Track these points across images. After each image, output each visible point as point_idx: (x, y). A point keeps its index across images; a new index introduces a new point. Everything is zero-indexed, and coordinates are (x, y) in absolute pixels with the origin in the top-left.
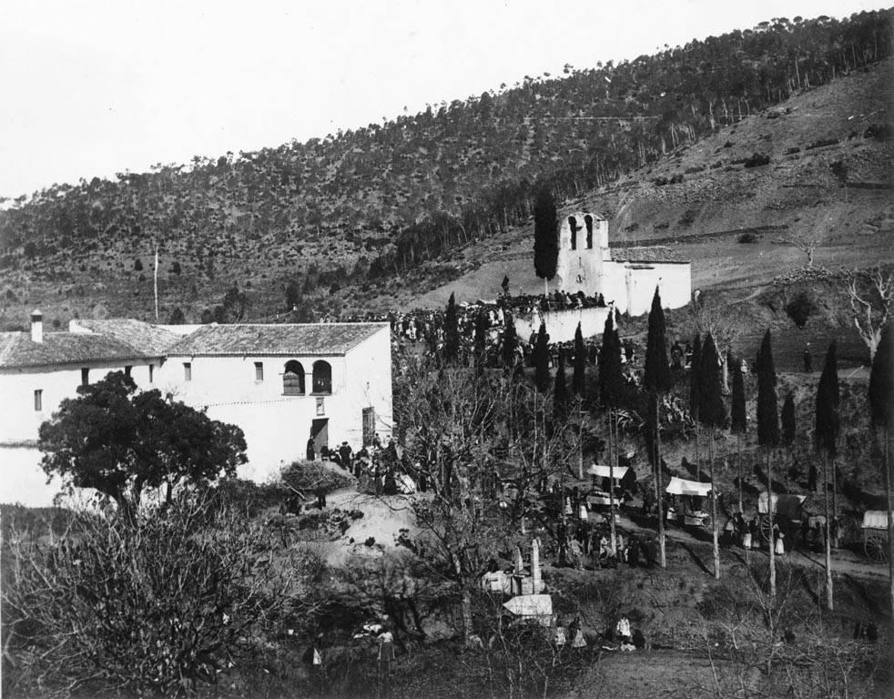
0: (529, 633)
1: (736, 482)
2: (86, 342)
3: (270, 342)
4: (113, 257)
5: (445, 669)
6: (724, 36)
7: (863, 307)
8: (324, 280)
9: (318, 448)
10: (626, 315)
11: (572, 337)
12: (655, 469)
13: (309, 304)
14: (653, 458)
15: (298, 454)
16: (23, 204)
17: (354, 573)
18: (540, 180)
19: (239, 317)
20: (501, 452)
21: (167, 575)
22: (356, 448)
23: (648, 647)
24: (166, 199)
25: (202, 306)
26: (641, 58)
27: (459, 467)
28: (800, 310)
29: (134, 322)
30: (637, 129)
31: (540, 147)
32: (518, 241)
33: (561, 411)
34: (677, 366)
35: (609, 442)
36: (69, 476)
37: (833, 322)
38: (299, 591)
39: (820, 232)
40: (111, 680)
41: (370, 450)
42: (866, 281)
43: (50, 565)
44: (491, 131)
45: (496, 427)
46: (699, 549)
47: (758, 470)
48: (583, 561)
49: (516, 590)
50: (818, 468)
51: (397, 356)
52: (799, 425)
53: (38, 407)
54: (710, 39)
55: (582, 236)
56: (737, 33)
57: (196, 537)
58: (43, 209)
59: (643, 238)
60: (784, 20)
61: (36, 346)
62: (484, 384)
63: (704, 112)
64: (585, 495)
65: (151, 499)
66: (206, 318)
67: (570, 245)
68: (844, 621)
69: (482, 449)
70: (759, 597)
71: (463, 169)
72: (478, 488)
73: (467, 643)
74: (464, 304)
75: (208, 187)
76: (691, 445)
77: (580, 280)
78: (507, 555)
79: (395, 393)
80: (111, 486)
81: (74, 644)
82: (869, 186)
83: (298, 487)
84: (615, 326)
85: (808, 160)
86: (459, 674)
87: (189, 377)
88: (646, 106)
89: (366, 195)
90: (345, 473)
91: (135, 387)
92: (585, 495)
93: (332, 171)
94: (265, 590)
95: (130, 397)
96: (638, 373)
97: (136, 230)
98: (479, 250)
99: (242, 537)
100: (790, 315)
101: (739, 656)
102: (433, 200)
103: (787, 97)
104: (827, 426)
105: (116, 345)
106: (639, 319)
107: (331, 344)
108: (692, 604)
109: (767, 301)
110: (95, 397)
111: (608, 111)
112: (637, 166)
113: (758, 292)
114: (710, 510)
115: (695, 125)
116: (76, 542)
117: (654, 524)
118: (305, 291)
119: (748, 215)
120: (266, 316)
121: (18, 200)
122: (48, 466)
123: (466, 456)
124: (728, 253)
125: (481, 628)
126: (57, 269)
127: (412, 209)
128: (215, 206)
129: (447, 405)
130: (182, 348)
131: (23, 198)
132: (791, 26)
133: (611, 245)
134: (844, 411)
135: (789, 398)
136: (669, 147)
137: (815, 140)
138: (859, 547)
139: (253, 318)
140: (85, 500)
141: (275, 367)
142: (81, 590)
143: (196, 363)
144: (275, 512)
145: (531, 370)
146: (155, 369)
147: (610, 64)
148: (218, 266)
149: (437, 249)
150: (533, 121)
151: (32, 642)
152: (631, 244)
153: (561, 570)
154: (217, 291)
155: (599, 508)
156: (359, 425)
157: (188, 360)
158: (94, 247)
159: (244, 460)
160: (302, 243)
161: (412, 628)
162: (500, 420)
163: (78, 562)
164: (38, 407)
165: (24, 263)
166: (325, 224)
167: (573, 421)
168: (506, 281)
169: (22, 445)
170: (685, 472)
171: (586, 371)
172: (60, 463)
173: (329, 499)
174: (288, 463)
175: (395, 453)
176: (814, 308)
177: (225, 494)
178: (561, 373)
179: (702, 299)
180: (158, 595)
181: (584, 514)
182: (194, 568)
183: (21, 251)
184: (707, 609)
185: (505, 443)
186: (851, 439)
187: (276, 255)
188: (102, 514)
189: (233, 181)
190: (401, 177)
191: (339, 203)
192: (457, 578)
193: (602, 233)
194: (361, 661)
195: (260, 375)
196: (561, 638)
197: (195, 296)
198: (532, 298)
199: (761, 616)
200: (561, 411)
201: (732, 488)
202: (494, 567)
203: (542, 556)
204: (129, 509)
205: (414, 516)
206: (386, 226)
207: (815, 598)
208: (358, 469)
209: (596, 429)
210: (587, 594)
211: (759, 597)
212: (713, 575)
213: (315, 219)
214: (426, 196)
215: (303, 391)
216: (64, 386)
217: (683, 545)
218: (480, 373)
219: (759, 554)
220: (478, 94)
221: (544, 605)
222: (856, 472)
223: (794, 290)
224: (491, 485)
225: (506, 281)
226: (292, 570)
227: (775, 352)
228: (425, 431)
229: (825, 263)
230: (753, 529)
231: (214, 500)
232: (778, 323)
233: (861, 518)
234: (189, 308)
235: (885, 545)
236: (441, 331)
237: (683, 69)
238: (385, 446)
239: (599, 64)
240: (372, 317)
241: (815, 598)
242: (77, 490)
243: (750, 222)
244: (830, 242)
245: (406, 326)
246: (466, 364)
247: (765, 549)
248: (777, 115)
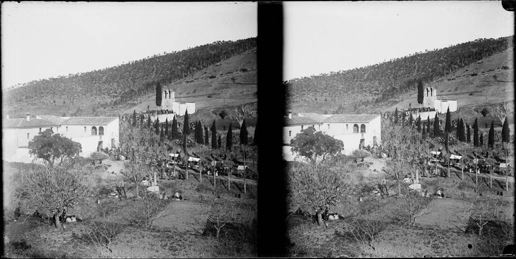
0: (153, 196)
1: (206, 158)
2: (41, 121)
4: (48, 99)
5: (394, 203)
6: (205, 45)
7: (239, 114)
8: (102, 106)
9: (100, 149)
11: (427, 119)
12: (186, 155)
13: (98, 112)
14: (447, 149)
15: (95, 150)
16: (25, 85)
17: (109, 181)
18: (419, 79)
19: (80, 115)
20: (147, 150)
21: (61, 181)
22: (372, 147)
23: (445, 197)
24: (62, 84)
25: (332, 110)
27: (398, 151)
28: (222, 115)
30: (182, 68)
31: (419, 70)
32: (151, 96)
33: (424, 138)
34: (191, 128)
35: (174, 147)
36: (36, 155)
37: (231, 118)
38: (95, 185)
39: (228, 95)
40: (309, 205)
41: (375, 147)
42: (239, 107)
43: (31, 178)
44: (145, 69)
45: (146, 144)
46: (459, 173)
47: (473, 153)
48: (429, 175)
49: (150, 185)
50: (489, 152)
51: (120, 125)
52: (222, 144)
53: (28, 137)
54: (463, 44)
56: (208, 44)
57: (68, 171)
58: (30, 87)
59: (183, 96)
60: (481, 39)
61: (28, 122)
62: (405, 130)
63: (461, 62)
64: (168, 161)
65: (57, 161)
66: (72, 115)
67: (430, 95)
68: (233, 193)
69: (142, 149)
70: (211, 187)
71: (138, 78)
72: (141, 159)
73: (400, 196)
74: (400, 110)
75: (334, 79)
76: (195, 149)
77: (429, 104)
78: (410, 174)
79: (382, 132)
80: (47, 158)
81: (37, 198)
82: (241, 84)
83: (95, 160)
84: (176, 118)
85: (487, 75)
86: (398, 204)
87: (329, 128)
88: (446, 60)
89: (113, 84)
90: (107, 155)
91: (53, 133)
92: (168, 161)
93: (104, 79)
94: (86, 184)
95: (314, 133)
96: (443, 128)
97: (316, 90)
98: (142, 99)
99: (343, 169)
100: (220, 116)
101: (206, 202)
102: (130, 86)
103: (482, 58)
104: (491, 142)
105: (309, 119)
106: (444, 114)
107: (366, 120)
108: (194, 189)
109: (214, 113)
110: (43, 135)
111: (175, 63)
112: (182, 78)
113: (212, 110)
114: (199, 165)
115: (459, 65)
116: (38, 172)
117: (447, 166)
118: (359, 107)
119: (472, 88)
120: (87, 115)
121: (24, 84)
122: (31, 153)
123: (138, 151)
124: (205, 100)
125: (403, 192)
126: (34, 102)
127: (386, 86)
128: (74, 87)
129: (133, 138)
131: (25, 84)
132: (483, 41)
133: (175, 98)
134: (496, 138)
135: (220, 137)
136: (190, 73)
137: (227, 72)
138: (236, 175)
139: (84, 115)
140: (40, 161)
141: (89, 128)
142: (38, 184)
143: (69, 127)
144: (89, 165)
145: (417, 127)
146: (59, 128)
148: (336, 99)
149: (131, 98)
150: (418, 64)
151: (26, 198)
152: (180, 97)
153: (423, 178)
154: (75, 108)
155: (171, 164)
156: (110, 143)
157: (67, 126)
158: (43, 96)
159: (81, 151)
160: (97, 96)
161: (385, 192)
162: (147, 142)
163: (38, 177)
164: (28, 137)
165: (25, 100)
166: (364, 89)
167: (165, 142)
168: (148, 107)
169: (24, 147)
170: (193, 155)
171: (430, 127)
172: (34, 152)
173: (364, 159)
174: (93, 152)
175: (119, 150)
176: (226, 114)
177: (76, 160)
178: (162, 130)
179: (198, 112)
180: (59, 186)
181: (167, 166)
182: (68, 179)
183: (24, 97)
184: (460, 188)
185: (148, 148)
186: (235, 147)
187: (90, 99)
188: (307, 163)
189: (341, 78)
190: (122, 80)
191: (368, 84)
192: (135, 182)
193: (435, 92)
194: (110, 203)
195: (347, 128)
196: (161, 197)
197: (69, 109)
198: (417, 109)
199: (474, 190)
200: (424, 138)
201: (467, 157)
202: (144, 179)
203: (157, 176)
204: (51, 164)
205: (124, 166)
206: (118, 92)
207: (225, 187)
208: (372, 152)
209: (171, 145)
210: (169, 186)
211: (211, 187)
212: (462, 179)
213: (100, 90)
214: (390, 82)
215: (358, 132)
216: (35, 132)
217: (454, 172)
218: (142, 130)
219: (212, 176)
220: (142, 59)
221: (419, 186)
222: (236, 156)
223: (222, 110)
224: (144, 158)
225: (148, 107)
226: (93, 180)
227: (216, 125)
228: (127, 144)
229: (229, 103)
230: (472, 167)
231: (336, 159)
232: (217, 118)
233: (237, 167)
234: (68, 113)
235: (243, 174)
236: (132, 119)
237: (456, 51)
238: (379, 146)
240: (114, 115)
241: (488, 185)
242: (38, 159)
243: (210, 92)
244: (231, 97)
245: (123, 118)
246: (138, 127)
247: (213, 175)
248: (218, 65)
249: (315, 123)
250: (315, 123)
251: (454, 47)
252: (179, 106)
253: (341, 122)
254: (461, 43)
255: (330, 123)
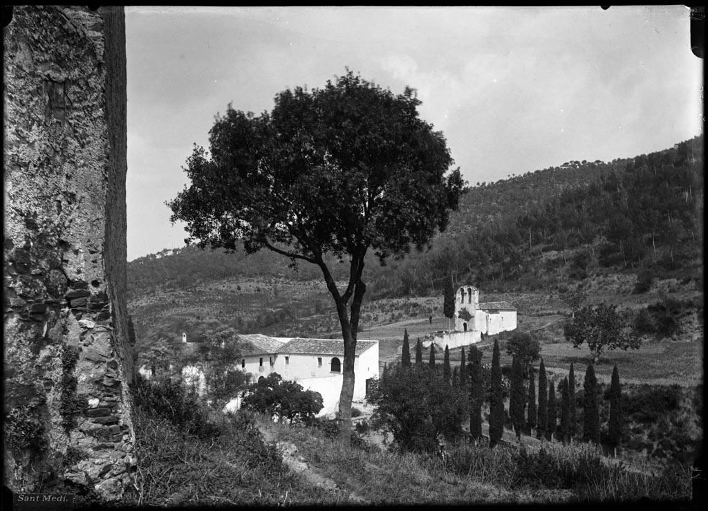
3: (325, 348)
6: (545, 170)
10: (486, 334)
26: (501, 181)
29: (261, 335)
55: (466, 298)
60: (577, 162)
87: (287, 363)
91: (281, 378)
130: (286, 352)
141: (327, 361)
143: (291, 358)
147: (484, 184)
239: (478, 184)
249: (264, 355)
250: (264, 355)
251: (519, 178)
252: (487, 317)
253: (308, 353)
254: (533, 171)
255: (290, 354)
